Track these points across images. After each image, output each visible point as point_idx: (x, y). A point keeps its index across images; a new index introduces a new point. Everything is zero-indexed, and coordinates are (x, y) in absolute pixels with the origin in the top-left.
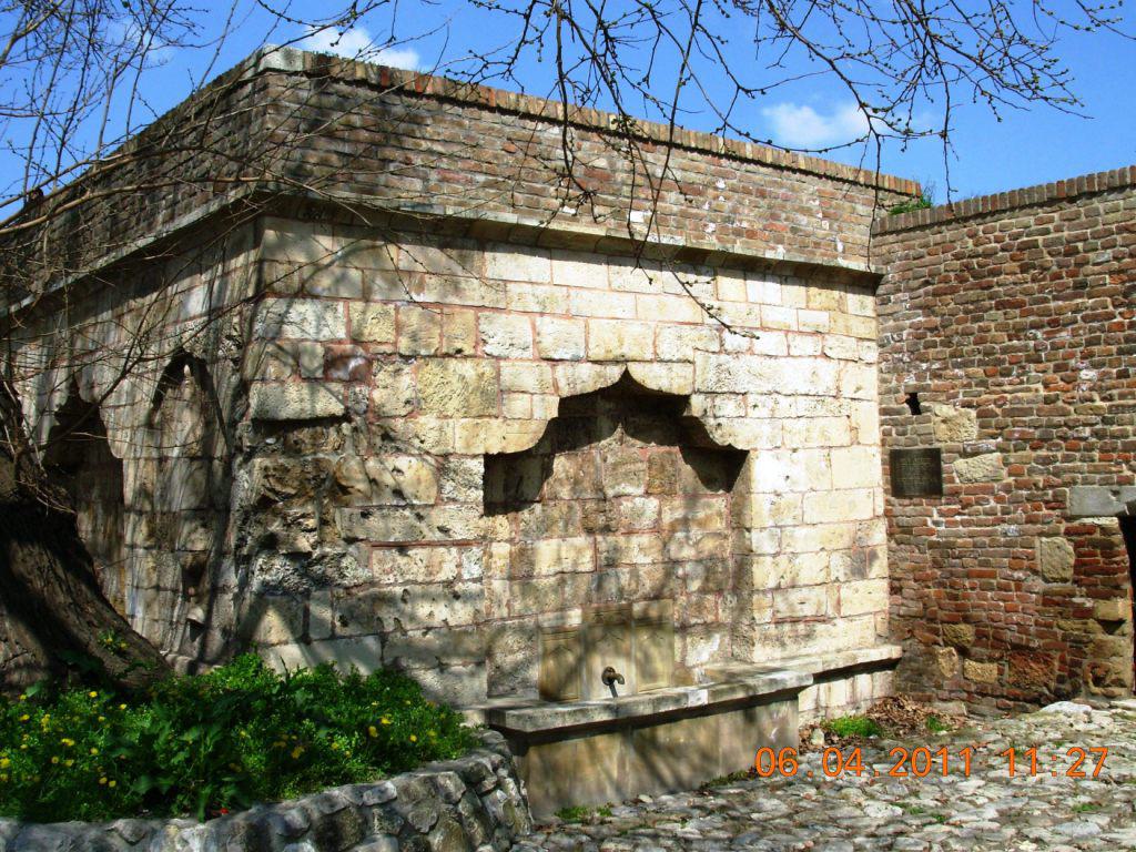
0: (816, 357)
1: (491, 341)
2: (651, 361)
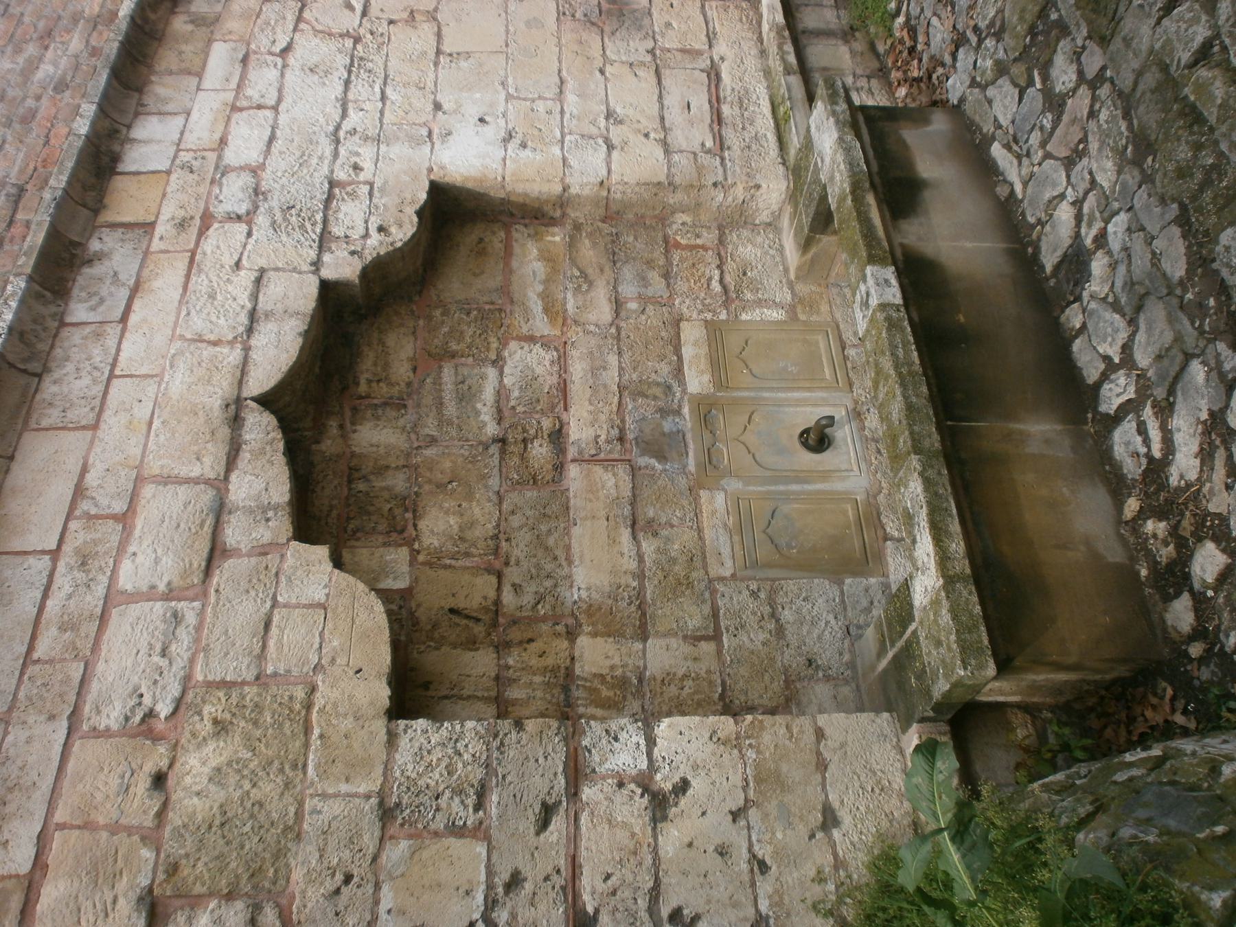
0: (285, 66)
1: (147, 700)
2: (247, 349)
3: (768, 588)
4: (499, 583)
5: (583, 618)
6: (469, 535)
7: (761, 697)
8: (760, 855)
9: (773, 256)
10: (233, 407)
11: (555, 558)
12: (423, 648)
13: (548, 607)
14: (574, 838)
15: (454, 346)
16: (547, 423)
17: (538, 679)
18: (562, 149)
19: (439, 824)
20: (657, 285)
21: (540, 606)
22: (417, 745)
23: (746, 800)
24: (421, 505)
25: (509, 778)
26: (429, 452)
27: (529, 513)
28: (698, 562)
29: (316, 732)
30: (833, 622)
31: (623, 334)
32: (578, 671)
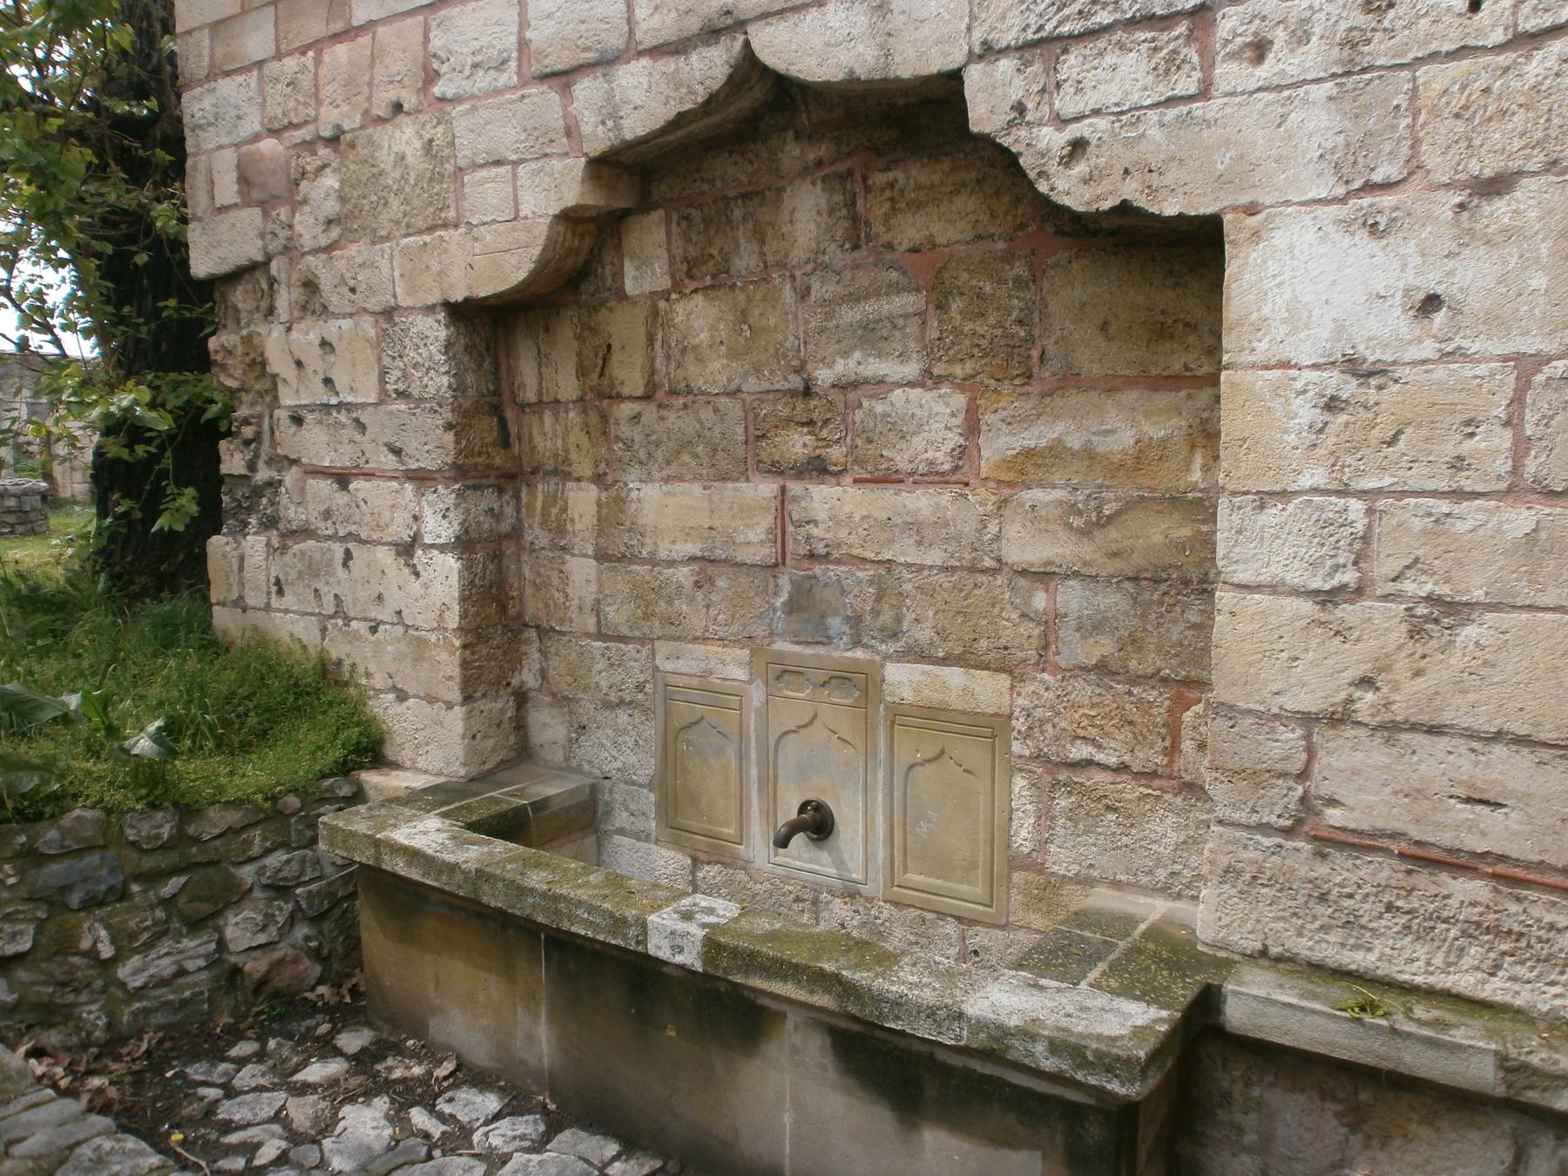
4: (639, 398)
5: (612, 492)
6: (690, 357)
9: (1150, 872)
10: (730, 21)
11: (668, 463)
12: (575, 320)
15: (956, 305)
16: (836, 453)
17: (559, 443)
18: (1315, 490)
19: (387, 361)
20: (1078, 649)
26: (788, 294)
27: (717, 430)
28: (670, 630)
29: (427, 238)
31: (982, 578)
32: (570, 485)
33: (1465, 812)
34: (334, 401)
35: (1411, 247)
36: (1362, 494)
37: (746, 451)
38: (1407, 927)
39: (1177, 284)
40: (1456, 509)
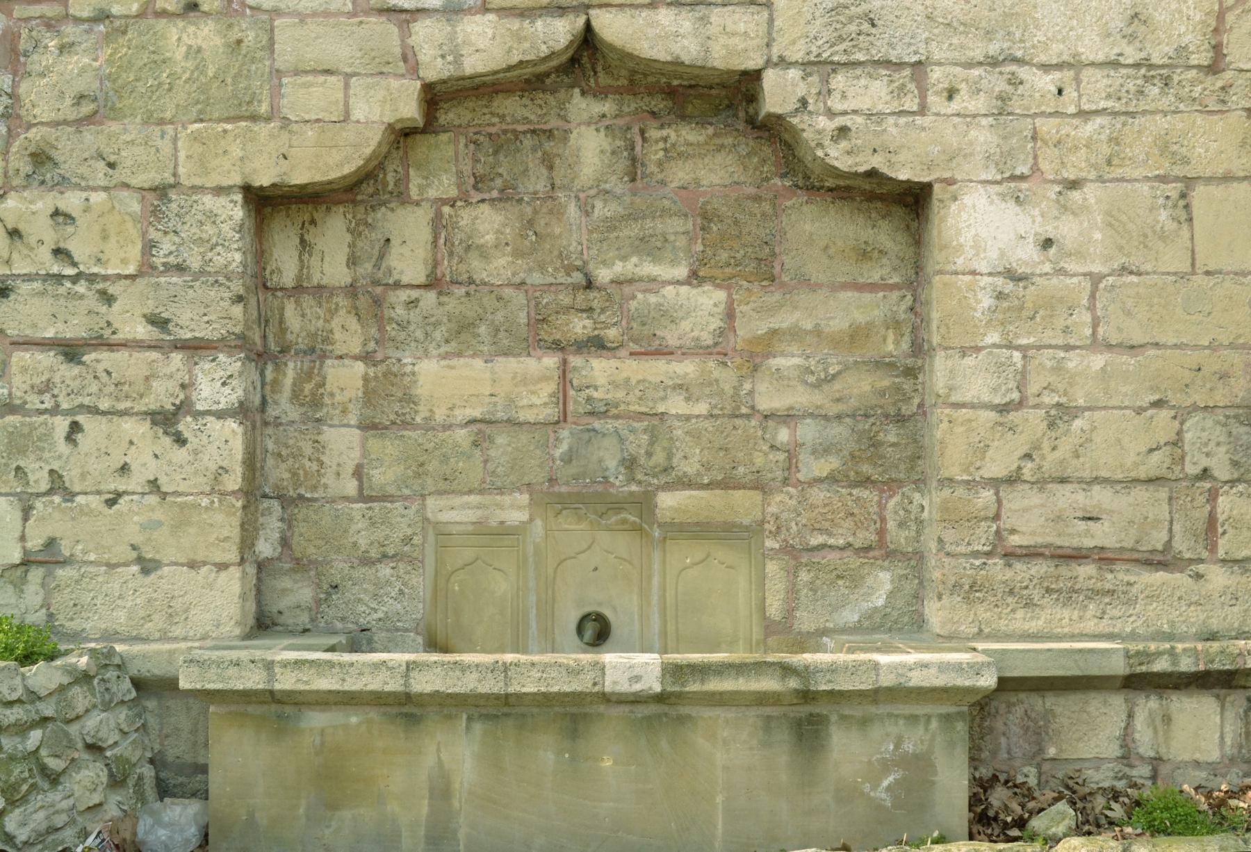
3: (415, 555)
4: (418, 287)
5: (381, 369)
7: (301, 535)
8: (121, 501)
12: (349, 216)
13: (393, 333)
14: (139, 345)
16: (612, 333)
18: (994, 346)
19: (153, 234)
21: (394, 325)
22: (219, 212)
23: (166, 494)
24: (508, 205)
25: (191, 291)
26: (572, 210)
29: (229, 127)
30: (375, 616)
31: (738, 422)
33: (1082, 525)
34: (70, 271)
35: (1036, 212)
36: (1018, 348)
37: (529, 331)
38: (1057, 599)
39: (874, 226)
40: (1067, 355)
